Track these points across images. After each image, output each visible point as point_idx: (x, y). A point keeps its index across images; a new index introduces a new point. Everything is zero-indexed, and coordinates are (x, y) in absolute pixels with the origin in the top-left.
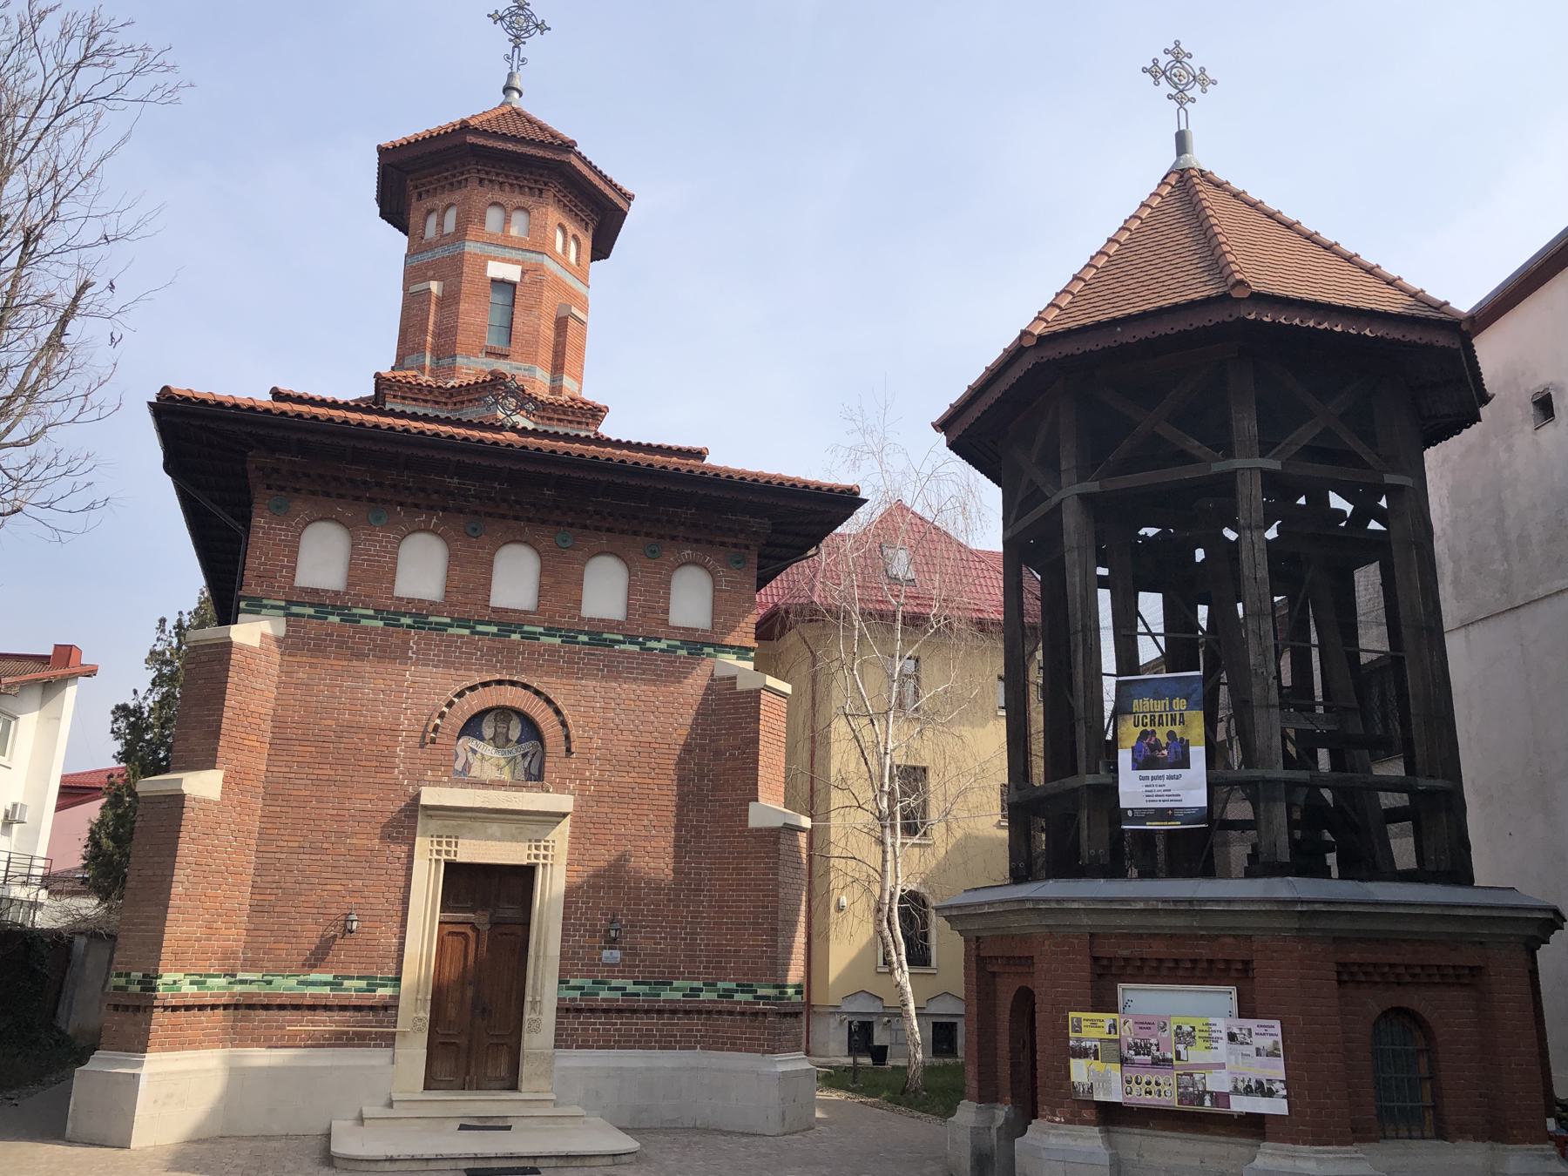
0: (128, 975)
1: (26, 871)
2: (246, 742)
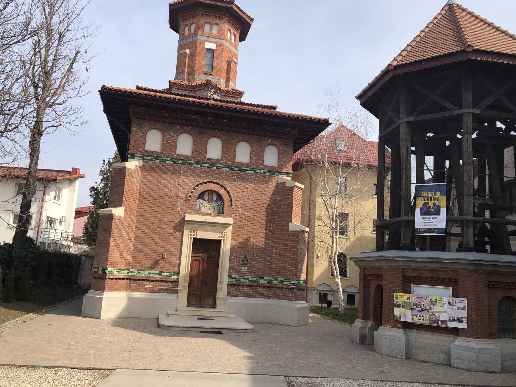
0: (98, 268)
1: (67, 236)
2: (131, 199)
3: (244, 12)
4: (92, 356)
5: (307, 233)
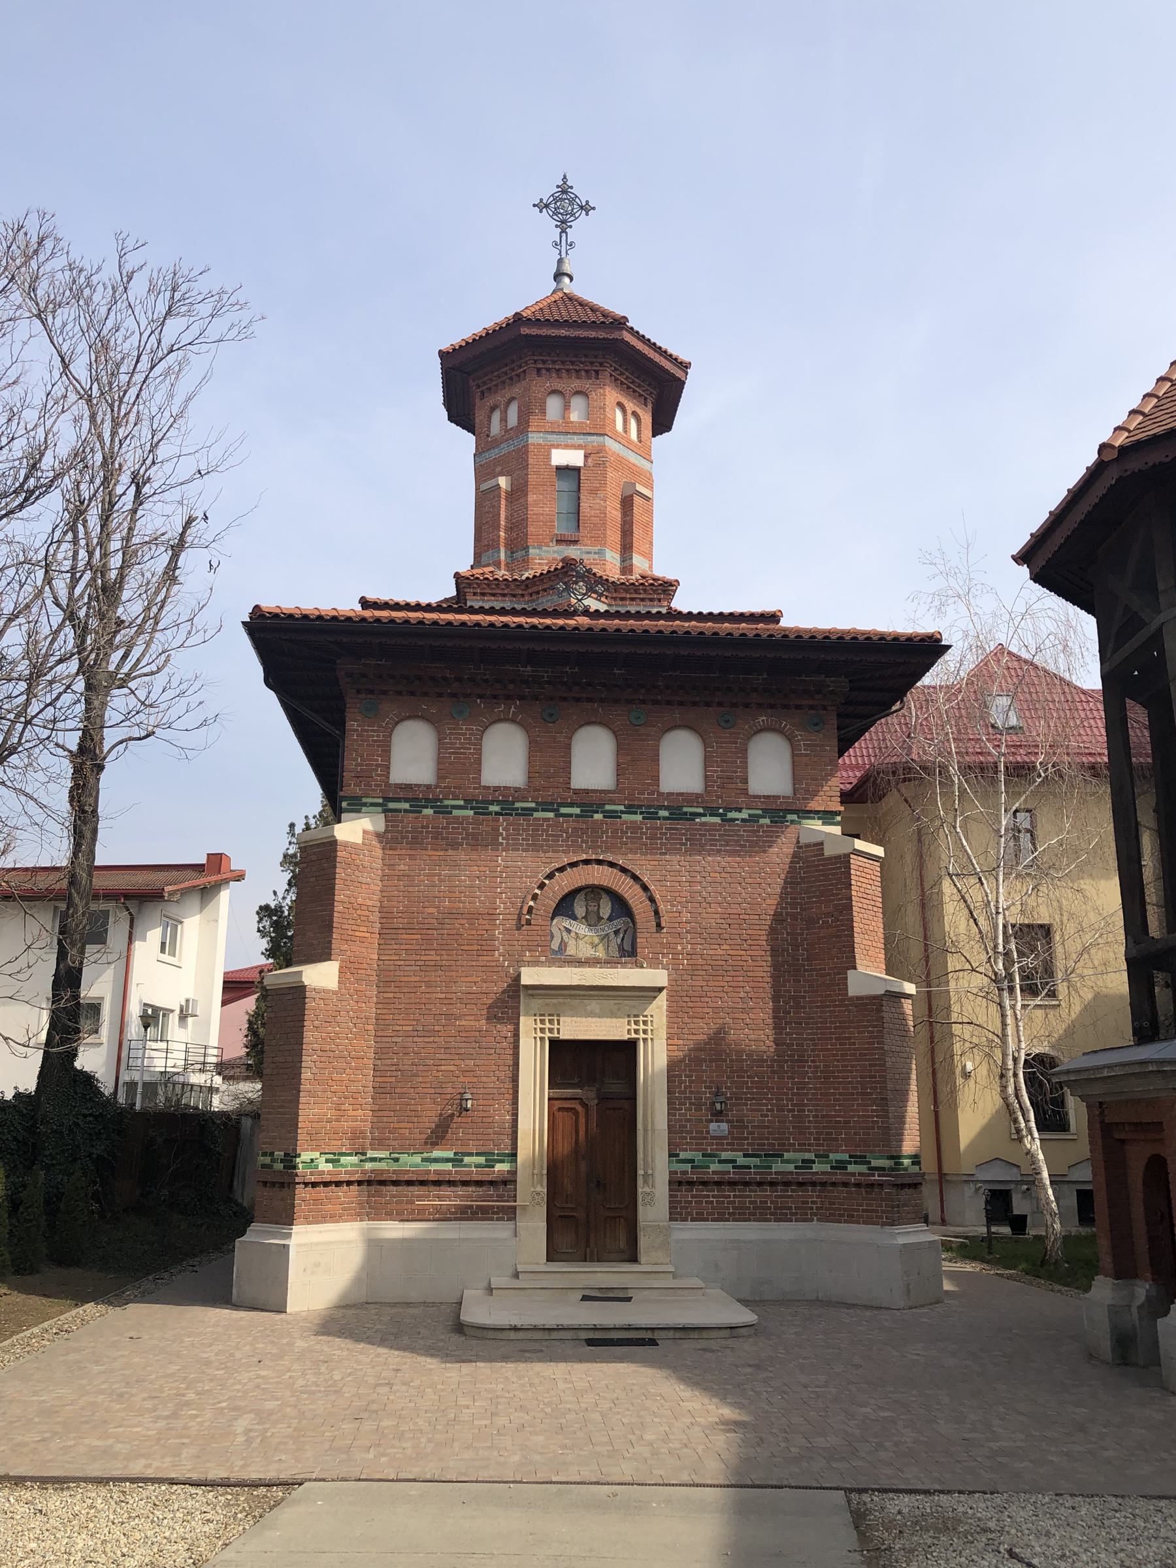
0: (272, 1154)
1: (201, 1059)
2: (357, 934)
3: (660, 348)
4: (241, 1439)
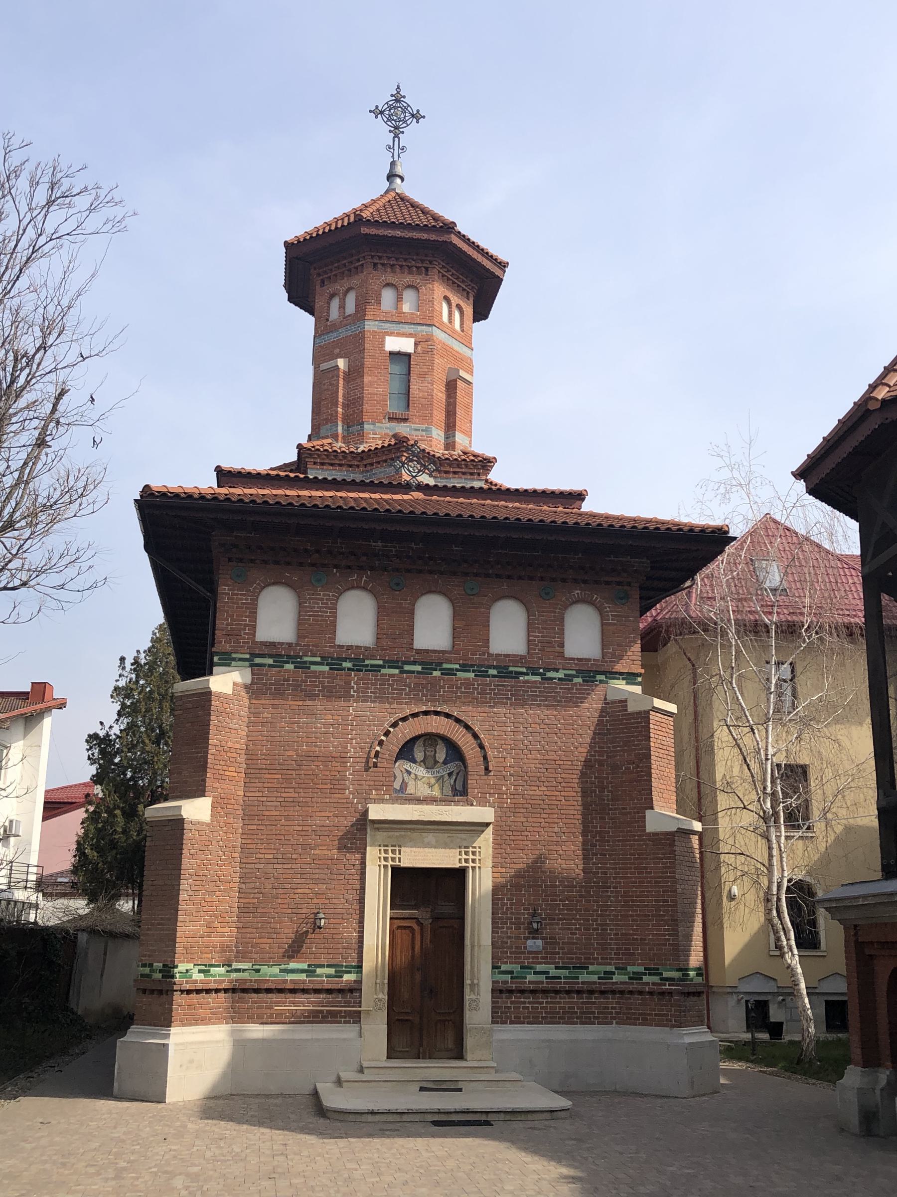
0: (151, 965)
1: (24, 877)
2: (227, 773)
5: (697, 837)
